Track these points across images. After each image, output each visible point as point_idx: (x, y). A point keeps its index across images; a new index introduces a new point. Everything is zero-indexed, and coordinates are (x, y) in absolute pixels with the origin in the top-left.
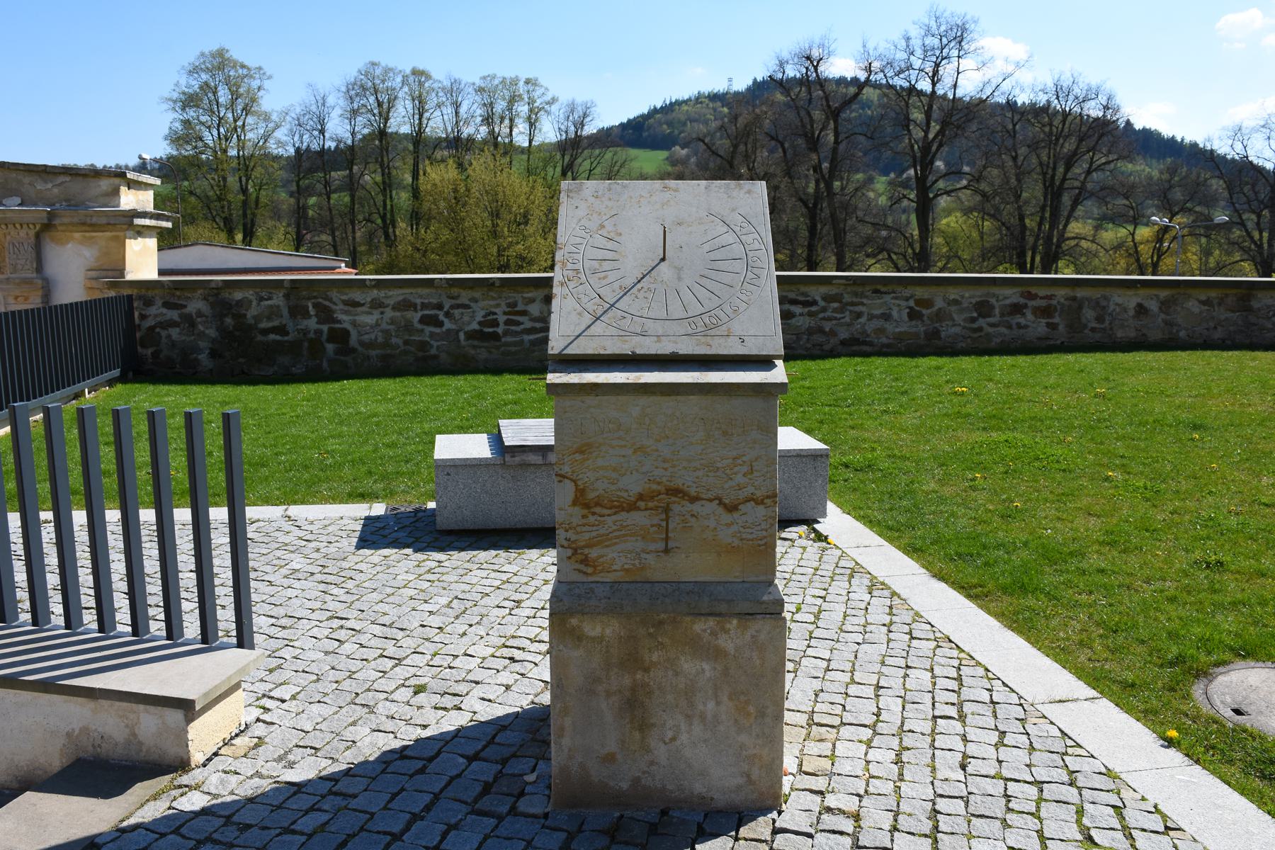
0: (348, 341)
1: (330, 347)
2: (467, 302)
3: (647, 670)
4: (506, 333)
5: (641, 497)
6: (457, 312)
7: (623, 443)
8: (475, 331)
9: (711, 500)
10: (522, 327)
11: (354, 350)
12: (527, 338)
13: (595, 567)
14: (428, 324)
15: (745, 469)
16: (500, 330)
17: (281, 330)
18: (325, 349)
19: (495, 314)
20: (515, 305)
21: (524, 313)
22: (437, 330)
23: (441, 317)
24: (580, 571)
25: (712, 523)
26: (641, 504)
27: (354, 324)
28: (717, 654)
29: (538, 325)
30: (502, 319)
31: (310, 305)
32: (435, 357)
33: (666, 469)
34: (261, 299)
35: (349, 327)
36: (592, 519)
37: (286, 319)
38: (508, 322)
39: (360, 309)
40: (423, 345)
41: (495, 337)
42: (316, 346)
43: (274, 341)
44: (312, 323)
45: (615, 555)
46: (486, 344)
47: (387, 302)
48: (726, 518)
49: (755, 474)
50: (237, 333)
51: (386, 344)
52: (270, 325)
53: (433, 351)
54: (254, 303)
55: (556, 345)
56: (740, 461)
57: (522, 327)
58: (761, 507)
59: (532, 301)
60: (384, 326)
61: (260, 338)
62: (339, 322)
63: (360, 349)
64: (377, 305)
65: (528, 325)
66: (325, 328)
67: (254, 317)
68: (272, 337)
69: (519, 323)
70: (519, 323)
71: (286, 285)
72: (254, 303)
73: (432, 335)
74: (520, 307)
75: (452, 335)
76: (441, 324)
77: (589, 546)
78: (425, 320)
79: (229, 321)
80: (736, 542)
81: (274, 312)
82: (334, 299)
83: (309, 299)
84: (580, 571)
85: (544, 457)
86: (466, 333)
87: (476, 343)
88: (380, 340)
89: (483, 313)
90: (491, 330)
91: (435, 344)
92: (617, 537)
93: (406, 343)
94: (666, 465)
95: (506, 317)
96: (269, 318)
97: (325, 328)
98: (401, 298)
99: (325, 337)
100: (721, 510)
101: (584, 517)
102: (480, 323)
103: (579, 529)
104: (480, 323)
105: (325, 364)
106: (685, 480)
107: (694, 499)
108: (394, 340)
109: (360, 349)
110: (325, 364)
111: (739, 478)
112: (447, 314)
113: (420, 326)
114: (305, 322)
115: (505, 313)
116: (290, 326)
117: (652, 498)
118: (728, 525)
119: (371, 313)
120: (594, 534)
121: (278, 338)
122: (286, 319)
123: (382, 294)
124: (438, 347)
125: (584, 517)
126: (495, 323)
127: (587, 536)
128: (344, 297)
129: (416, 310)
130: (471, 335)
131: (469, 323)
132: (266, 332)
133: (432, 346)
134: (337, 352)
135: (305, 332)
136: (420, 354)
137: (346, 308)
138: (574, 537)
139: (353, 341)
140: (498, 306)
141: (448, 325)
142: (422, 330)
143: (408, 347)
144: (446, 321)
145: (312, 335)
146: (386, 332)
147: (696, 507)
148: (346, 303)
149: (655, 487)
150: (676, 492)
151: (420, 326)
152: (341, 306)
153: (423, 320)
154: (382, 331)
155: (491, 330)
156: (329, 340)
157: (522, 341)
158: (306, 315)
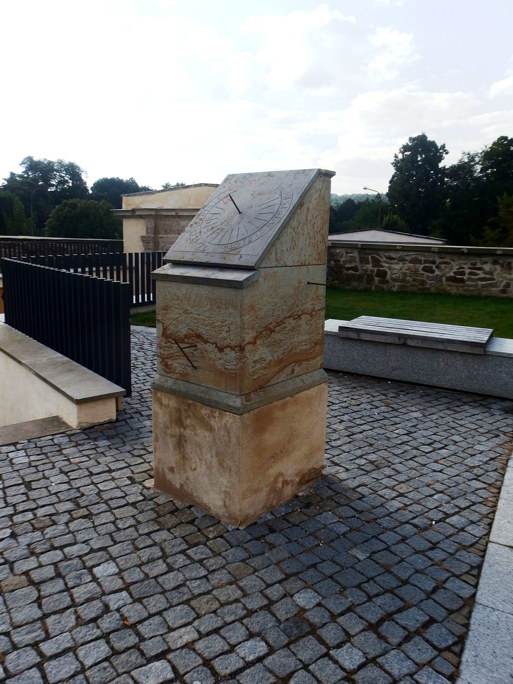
0: (385, 277)
1: (377, 279)
2: (449, 261)
3: (185, 428)
4: (469, 279)
5: (186, 336)
6: (443, 266)
7: (180, 307)
8: (451, 277)
9: (213, 344)
10: (478, 276)
11: (388, 282)
12: (480, 283)
13: (170, 369)
14: (427, 271)
15: (226, 329)
16: (465, 277)
17: (355, 269)
18: (374, 280)
19: (464, 268)
20: (475, 264)
21: (480, 269)
22: (431, 275)
23: (434, 268)
24: (165, 370)
25: (212, 356)
26: (186, 340)
27: (390, 268)
28: (211, 429)
29: (487, 276)
30: (467, 271)
31: (370, 257)
32: (428, 289)
33: (195, 323)
34: (348, 253)
35: (387, 270)
36: (169, 344)
37: (357, 264)
38: (470, 274)
39: (393, 261)
40: (423, 283)
41: (462, 281)
42: (370, 278)
43: (352, 274)
44: (370, 267)
45: (176, 365)
46: (455, 284)
47: (407, 258)
48: (219, 355)
49: (231, 332)
50: (335, 269)
51: (403, 280)
52: (350, 266)
53: (428, 286)
54: (344, 254)
55: (169, 255)
56: (224, 324)
57: (478, 276)
58: (233, 352)
59: (486, 263)
60: (404, 271)
61: (345, 272)
62: (383, 267)
63: (390, 281)
64: (402, 260)
65: (482, 275)
66: (376, 269)
67: (344, 261)
68: (351, 271)
69: (476, 275)
70: (476, 275)
71: (359, 246)
72: (344, 254)
73: (428, 277)
74: (478, 266)
75: (438, 279)
76: (433, 272)
77: (168, 358)
78: (425, 269)
79: (332, 262)
80: (223, 370)
81: (353, 259)
82: (381, 255)
83: (370, 254)
84: (165, 370)
85: (358, 335)
86: (446, 278)
87: (451, 283)
88: (401, 277)
89: (457, 267)
90: (460, 277)
91: (429, 282)
92: (177, 356)
93: (414, 280)
94: (195, 321)
95: (470, 270)
96: (350, 262)
97: (376, 269)
98: (414, 257)
99: (375, 273)
100: (216, 350)
101: (166, 343)
102: (455, 273)
103: (164, 348)
104: (455, 273)
105: (373, 288)
106: (202, 330)
107: (206, 342)
108: (408, 278)
109: (390, 281)
110: (373, 288)
111: (224, 334)
112: (437, 267)
113: (422, 272)
114: (367, 266)
115: (470, 268)
116: (359, 267)
117: (190, 338)
118: (220, 359)
119: (399, 264)
120: (169, 352)
121: (353, 272)
122: (357, 264)
123: (405, 253)
124: (430, 284)
125: (166, 343)
126: (463, 273)
127: (166, 353)
128: (386, 254)
129: (421, 264)
130: (449, 279)
131: (449, 272)
132: (348, 269)
133: (427, 283)
134: (380, 282)
135: (366, 271)
136: (420, 287)
137: (387, 260)
138: (163, 352)
139: (388, 277)
140: (466, 264)
141: (437, 272)
142: (423, 274)
143: (415, 283)
144: (436, 270)
145: (369, 272)
146: (404, 274)
147: (207, 346)
148: (387, 258)
149: (191, 332)
150: (199, 336)
151: (422, 272)
152: (385, 259)
153: (424, 269)
154: (402, 273)
155: (460, 277)
156: (376, 276)
157: (477, 284)
158: (367, 262)
